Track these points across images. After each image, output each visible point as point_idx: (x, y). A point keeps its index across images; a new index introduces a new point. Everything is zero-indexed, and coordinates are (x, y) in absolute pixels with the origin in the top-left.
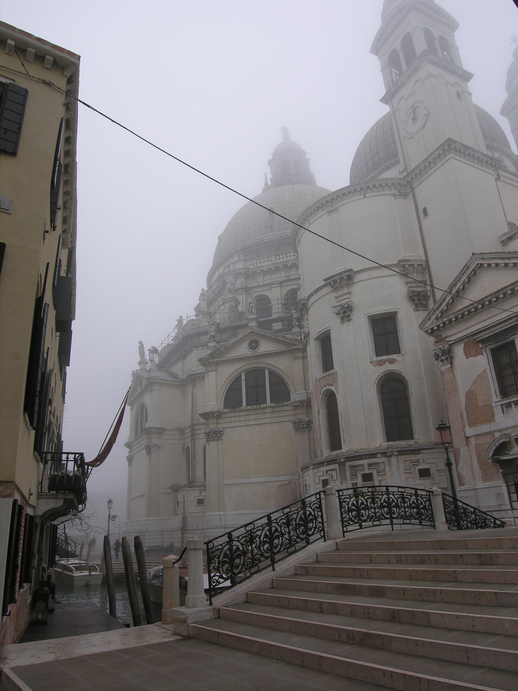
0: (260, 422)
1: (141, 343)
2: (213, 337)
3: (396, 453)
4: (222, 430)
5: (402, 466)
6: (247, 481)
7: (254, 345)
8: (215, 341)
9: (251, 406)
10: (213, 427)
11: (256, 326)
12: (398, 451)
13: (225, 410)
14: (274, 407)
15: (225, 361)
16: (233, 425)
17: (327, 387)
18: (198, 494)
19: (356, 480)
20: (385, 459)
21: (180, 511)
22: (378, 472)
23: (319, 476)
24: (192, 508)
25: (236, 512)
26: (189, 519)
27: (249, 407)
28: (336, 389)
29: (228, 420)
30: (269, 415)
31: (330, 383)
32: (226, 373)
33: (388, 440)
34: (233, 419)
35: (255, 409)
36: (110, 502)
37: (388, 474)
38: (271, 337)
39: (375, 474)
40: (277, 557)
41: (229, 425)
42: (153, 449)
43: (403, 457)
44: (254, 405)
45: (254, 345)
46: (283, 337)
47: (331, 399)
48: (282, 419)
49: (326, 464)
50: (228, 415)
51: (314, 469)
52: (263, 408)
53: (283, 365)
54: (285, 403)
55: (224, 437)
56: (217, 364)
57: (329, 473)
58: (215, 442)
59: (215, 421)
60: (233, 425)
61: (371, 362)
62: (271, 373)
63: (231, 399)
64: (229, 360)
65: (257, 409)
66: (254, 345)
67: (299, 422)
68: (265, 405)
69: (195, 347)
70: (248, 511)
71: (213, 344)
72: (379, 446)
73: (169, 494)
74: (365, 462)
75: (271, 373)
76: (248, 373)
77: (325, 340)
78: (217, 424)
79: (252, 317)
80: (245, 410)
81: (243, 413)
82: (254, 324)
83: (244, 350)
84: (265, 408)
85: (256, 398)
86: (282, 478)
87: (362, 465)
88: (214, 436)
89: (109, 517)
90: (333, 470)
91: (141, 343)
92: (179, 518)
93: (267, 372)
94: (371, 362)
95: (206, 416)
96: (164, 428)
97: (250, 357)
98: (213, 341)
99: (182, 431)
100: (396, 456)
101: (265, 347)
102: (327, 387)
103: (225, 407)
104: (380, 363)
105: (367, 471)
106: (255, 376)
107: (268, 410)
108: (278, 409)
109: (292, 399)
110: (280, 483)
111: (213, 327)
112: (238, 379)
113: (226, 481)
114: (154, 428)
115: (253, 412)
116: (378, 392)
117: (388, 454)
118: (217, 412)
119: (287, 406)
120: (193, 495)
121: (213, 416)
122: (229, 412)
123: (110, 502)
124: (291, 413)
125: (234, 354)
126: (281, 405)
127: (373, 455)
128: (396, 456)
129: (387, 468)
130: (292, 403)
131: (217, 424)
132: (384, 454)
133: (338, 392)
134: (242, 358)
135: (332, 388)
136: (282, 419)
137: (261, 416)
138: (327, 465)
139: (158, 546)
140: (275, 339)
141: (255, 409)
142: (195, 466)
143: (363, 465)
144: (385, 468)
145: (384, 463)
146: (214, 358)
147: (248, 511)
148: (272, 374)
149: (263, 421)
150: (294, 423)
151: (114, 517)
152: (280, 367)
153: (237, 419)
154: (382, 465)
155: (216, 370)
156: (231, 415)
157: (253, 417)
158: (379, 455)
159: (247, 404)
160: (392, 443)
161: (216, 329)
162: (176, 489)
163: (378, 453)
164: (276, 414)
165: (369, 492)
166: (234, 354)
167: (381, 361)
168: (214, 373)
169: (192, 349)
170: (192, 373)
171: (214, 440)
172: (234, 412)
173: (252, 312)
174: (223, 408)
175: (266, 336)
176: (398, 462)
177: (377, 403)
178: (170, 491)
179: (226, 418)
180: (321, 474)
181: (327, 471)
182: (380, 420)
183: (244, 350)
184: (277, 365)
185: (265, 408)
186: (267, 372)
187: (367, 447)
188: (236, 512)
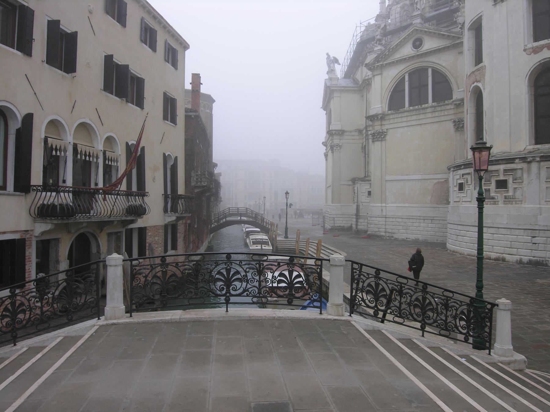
0: (420, 122)
1: (327, 54)
2: (380, 40)
3: (538, 159)
4: (385, 131)
5: (543, 174)
6: (406, 177)
7: (418, 43)
8: (381, 44)
9: (413, 106)
10: (377, 128)
11: (420, 23)
12: (541, 157)
13: (390, 112)
14: (435, 107)
15: (390, 63)
16: (396, 126)
17: (475, 84)
18: (369, 187)
19: (490, 186)
20: (524, 165)
21: (356, 201)
22: (515, 179)
23: (457, 179)
24: (363, 198)
25: (395, 205)
26: (361, 207)
27: (411, 108)
28: (483, 85)
29: (392, 121)
30: (429, 115)
31: (478, 79)
32: (392, 74)
33: (537, 143)
34: (396, 121)
35: (416, 110)
36: (287, 193)
37: (525, 182)
38: (435, 33)
39: (510, 181)
40: (233, 299)
41: (392, 126)
42: (335, 148)
43: (546, 163)
44: (416, 105)
45: (418, 43)
46: (447, 31)
47: (478, 96)
48: (442, 119)
49: (463, 167)
50: (391, 117)
51: (453, 171)
52: (423, 109)
53: (444, 62)
54: (446, 102)
55: (388, 137)
56: (382, 67)
57: (465, 177)
58: (380, 142)
59: (379, 123)
60: (396, 126)
61: (525, 50)
62: (435, 71)
63: (395, 101)
64: (393, 62)
65: (419, 109)
66: (418, 43)
67: (458, 121)
68: (426, 105)
69: (369, 52)
70: (406, 205)
71: (379, 47)
72: (522, 149)
73: (350, 185)
74: (501, 167)
75: (435, 71)
76: (412, 74)
77: (477, 28)
78: (381, 125)
79: (417, 13)
80: (407, 111)
81: (405, 114)
82: (418, 21)
83: (408, 50)
84: (427, 108)
85: (418, 99)
86: (438, 176)
87: (497, 171)
88: (380, 136)
89: (287, 205)
90: (468, 174)
91: (327, 54)
92: (355, 206)
93: (430, 71)
94: (525, 50)
95: (371, 118)
96: (343, 131)
97: (413, 57)
98: (379, 44)
99: (360, 131)
100: (538, 162)
101: (429, 44)
102: (475, 84)
103: (390, 109)
104: (536, 51)
105: (502, 178)
106: (417, 76)
107: (429, 110)
108: (439, 109)
109: (454, 97)
110: (437, 181)
111: (379, 30)
112: (402, 80)
113: (388, 178)
114: (335, 130)
115: (414, 113)
116: (529, 86)
117: (529, 160)
118: (380, 114)
119: (448, 104)
120: (364, 187)
121: (378, 118)
122: (392, 114)
123: (287, 193)
124: (452, 112)
125: (398, 56)
126: (443, 104)
127: (510, 160)
128: (538, 162)
129: (525, 176)
130: (453, 102)
131: (381, 125)
132: (523, 159)
133: (484, 89)
134: (405, 59)
135: (480, 85)
136: (442, 119)
137: (422, 116)
138: (464, 168)
139: (340, 226)
140: (439, 34)
141: (416, 110)
142: (368, 162)
143: (497, 170)
144: (522, 175)
145: (522, 169)
146: (378, 62)
147: (406, 205)
148: (436, 72)
149: (424, 121)
150: (454, 122)
151: (291, 205)
152: (444, 65)
153: (399, 120)
154: (519, 172)
155: (381, 74)
156: (396, 116)
157: (414, 118)
158: (517, 161)
159: (410, 105)
160: (539, 146)
161: (382, 32)
162: (354, 181)
163: (517, 158)
164: (437, 114)
165: (254, 260)
166: (398, 56)
167: (537, 47)
168: (379, 77)
169: (367, 54)
170: (366, 78)
171: (378, 141)
172: (396, 113)
173: (417, 8)
174: (387, 110)
175: (430, 32)
176: (539, 169)
177: (527, 100)
178: (350, 183)
179: (389, 119)
180: (458, 177)
181: (463, 175)
182: (527, 119)
183: (408, 50)
184: (440, 63)
185: (427, 108)
186: (430, 71)
187: (509, 151)
188: (395, 205)
